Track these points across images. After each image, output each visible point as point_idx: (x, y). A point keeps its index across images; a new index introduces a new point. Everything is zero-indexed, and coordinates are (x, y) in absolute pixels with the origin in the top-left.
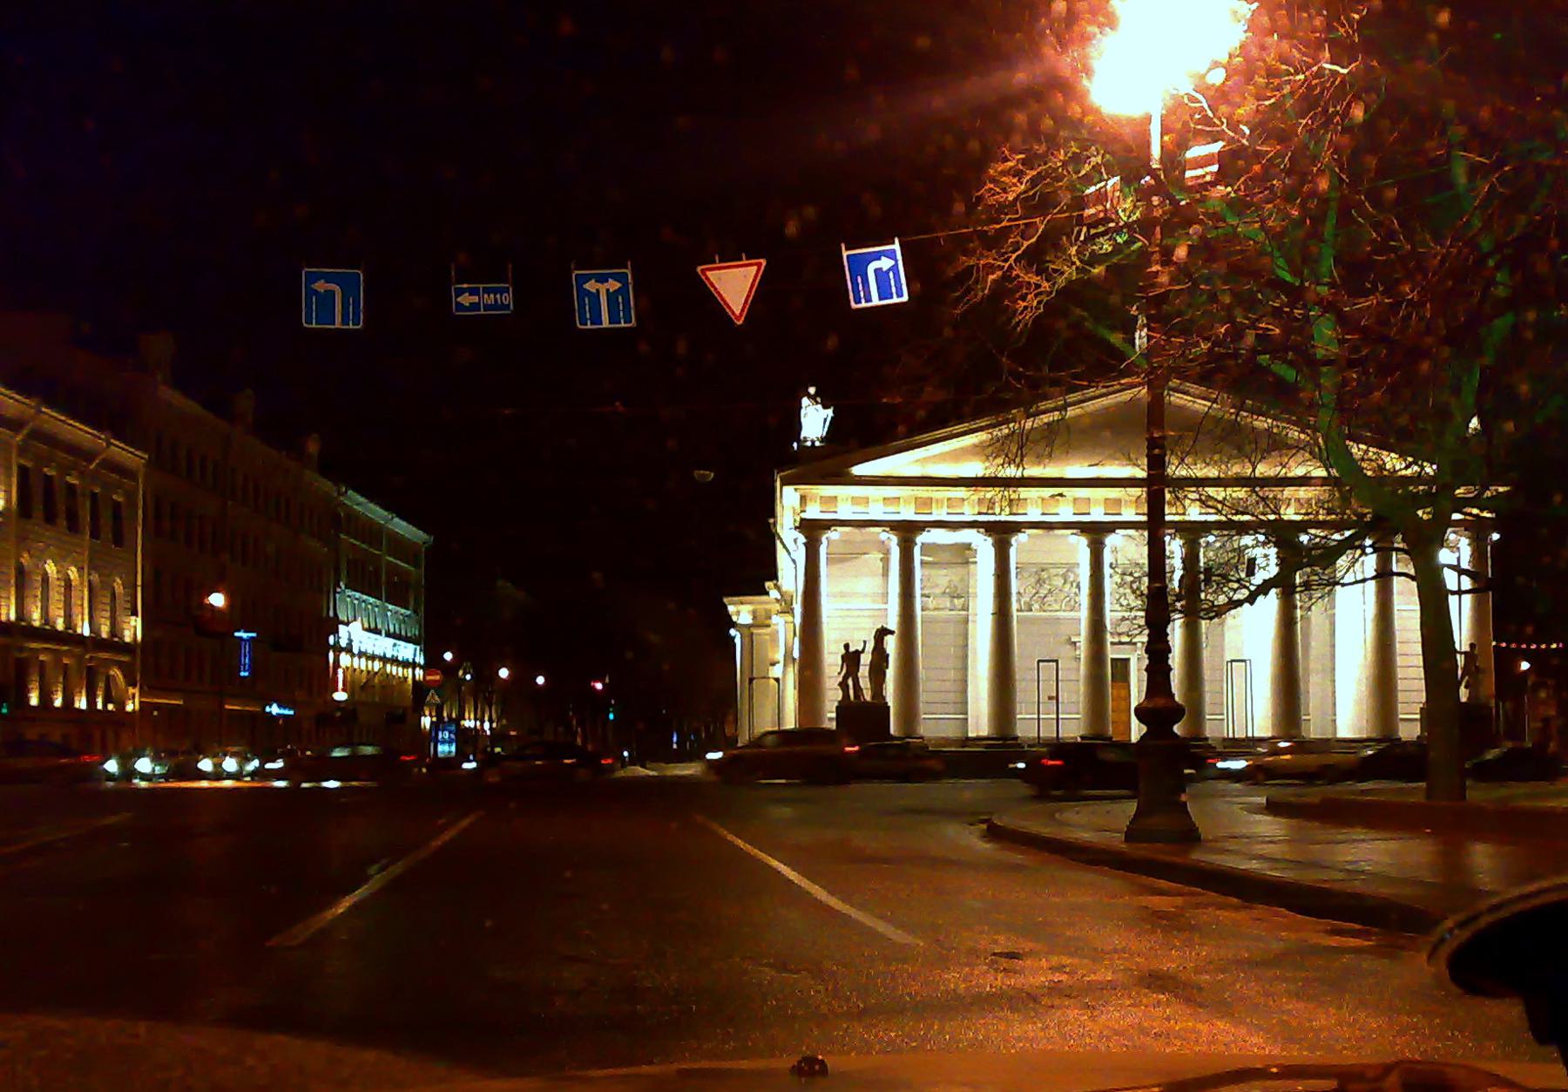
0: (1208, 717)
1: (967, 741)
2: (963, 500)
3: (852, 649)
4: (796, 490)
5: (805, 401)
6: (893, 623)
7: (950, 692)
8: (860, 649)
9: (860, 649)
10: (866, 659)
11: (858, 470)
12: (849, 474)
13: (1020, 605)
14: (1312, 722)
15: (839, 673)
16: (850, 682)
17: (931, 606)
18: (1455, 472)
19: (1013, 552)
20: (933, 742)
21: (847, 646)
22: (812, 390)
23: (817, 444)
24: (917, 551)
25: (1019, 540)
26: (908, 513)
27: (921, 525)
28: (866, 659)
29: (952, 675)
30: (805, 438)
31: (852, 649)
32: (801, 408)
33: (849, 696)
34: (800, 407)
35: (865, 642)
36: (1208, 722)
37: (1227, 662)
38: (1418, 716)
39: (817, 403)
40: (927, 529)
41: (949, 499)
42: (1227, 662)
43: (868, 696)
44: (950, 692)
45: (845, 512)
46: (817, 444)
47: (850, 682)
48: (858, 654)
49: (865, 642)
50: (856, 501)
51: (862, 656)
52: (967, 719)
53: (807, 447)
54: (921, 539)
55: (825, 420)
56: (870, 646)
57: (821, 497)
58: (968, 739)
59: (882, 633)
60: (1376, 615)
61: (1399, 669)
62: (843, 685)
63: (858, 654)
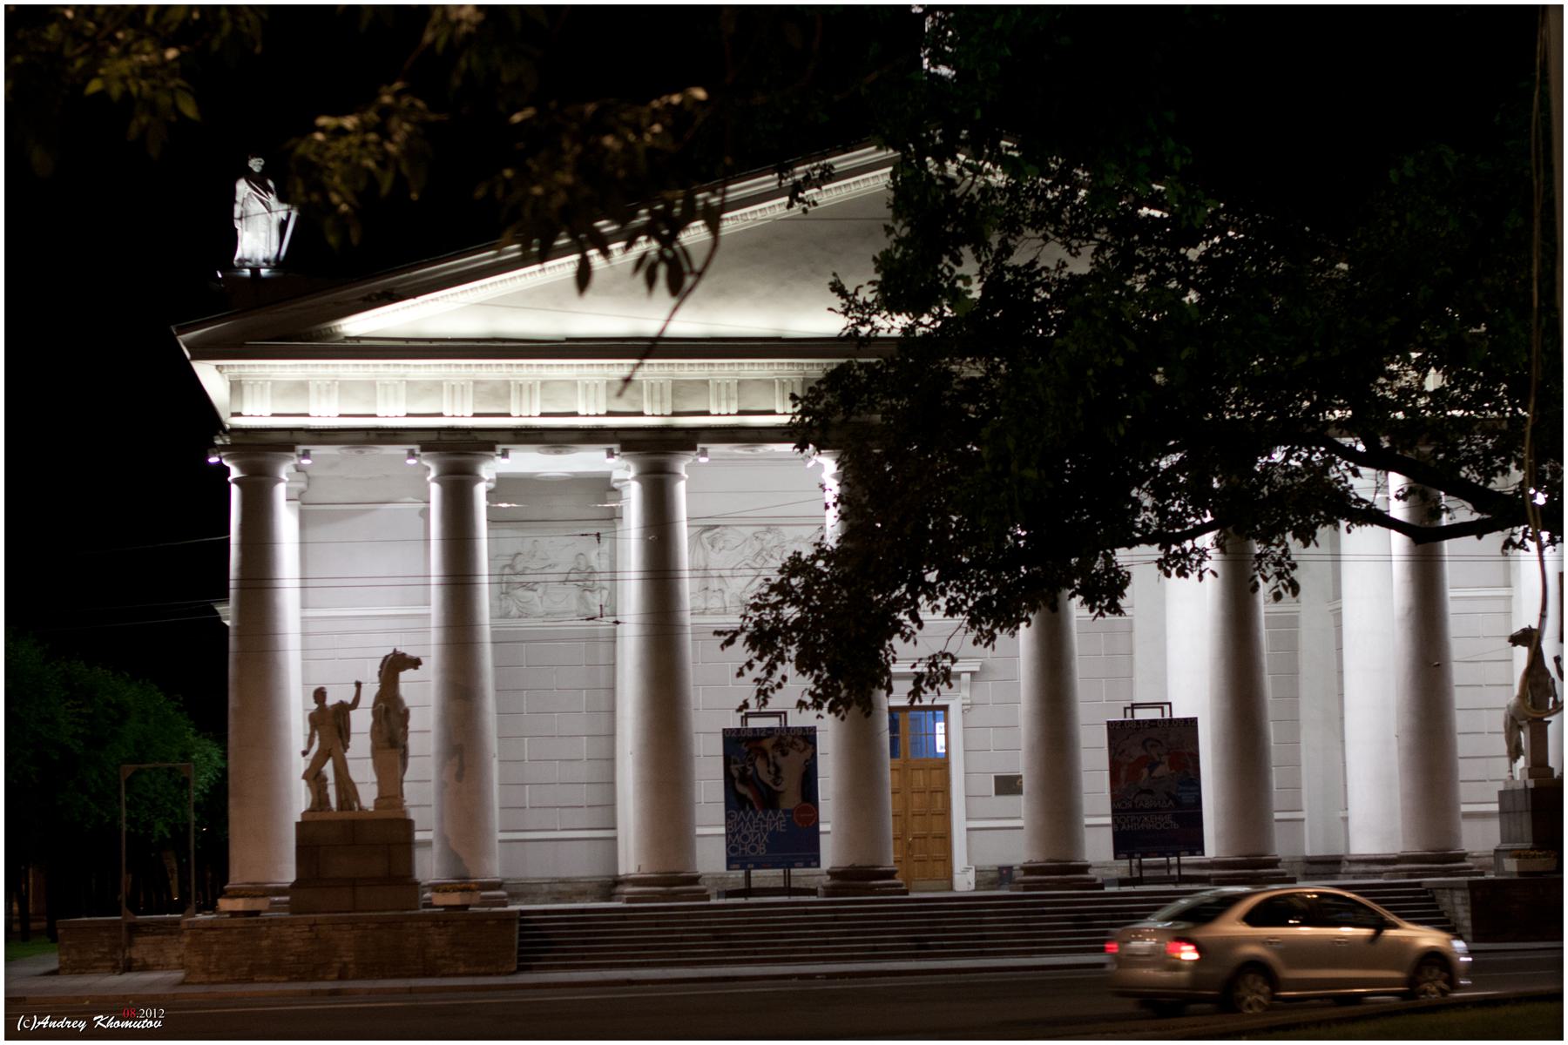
0: (1277, 816)
1: (611, 886)
2: (574, 384)
3: (331, 701)
4: (217, 366)
5: (242, 187)
6: (428, 644)
7: (584, 783)
8: (349, 700)
9: (349, 700)
10: (361, 721)
11: (355, 325)
12: (331, 335)
13: (724, 602)
14: (1306, 822)
15: (305, 753)
16: (329, 769)
17: (540, 609)
18: (1115, 246)
19: (681, 489)
20: (546, 887)
21: (320, 695)
22: (256, 164)
23: (264, 272)
24: (481, 491)
25: (687, 470)
26: (460, 414)
27: (488, 437)
28: (361, 721)
29: (583, 747)
30: (241, 260)
31: (331, 701)
32: (234, 201)
33: (327, 802)
34: (232, 200)
35: (358, 685)
36: (1276, 824)
37: (1125, 709)
38: (1495, 807)
39: (267, 189)
40: (500, 448)
41: (544, 384)
42: (1125, 709)
43: (368, 796)
44: (584, 783)
45: (324, 414)
46: (264, 272)
47: (329, 769)
48: (343, 710)
49: (358, 685)
50: (345, 388)
51: (354, 715)
52: (615, 839)
53: (245, 279)
54: (491, 469)
55: (283, 226)
56: (371, 689)
57: (274, 383)
58: (617, 882)
59: (396, 664)
60: (1410, 609)
61: (1457, 712)
62: (314, 777)
63: (343, 710)
